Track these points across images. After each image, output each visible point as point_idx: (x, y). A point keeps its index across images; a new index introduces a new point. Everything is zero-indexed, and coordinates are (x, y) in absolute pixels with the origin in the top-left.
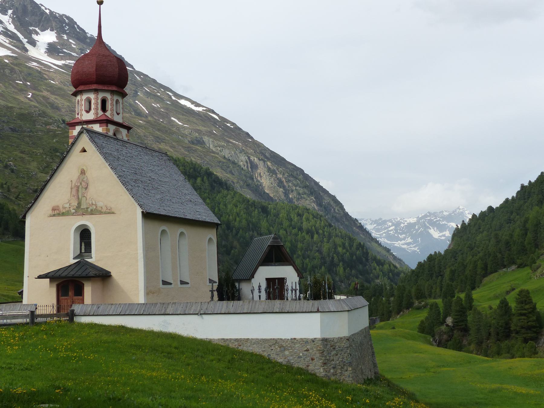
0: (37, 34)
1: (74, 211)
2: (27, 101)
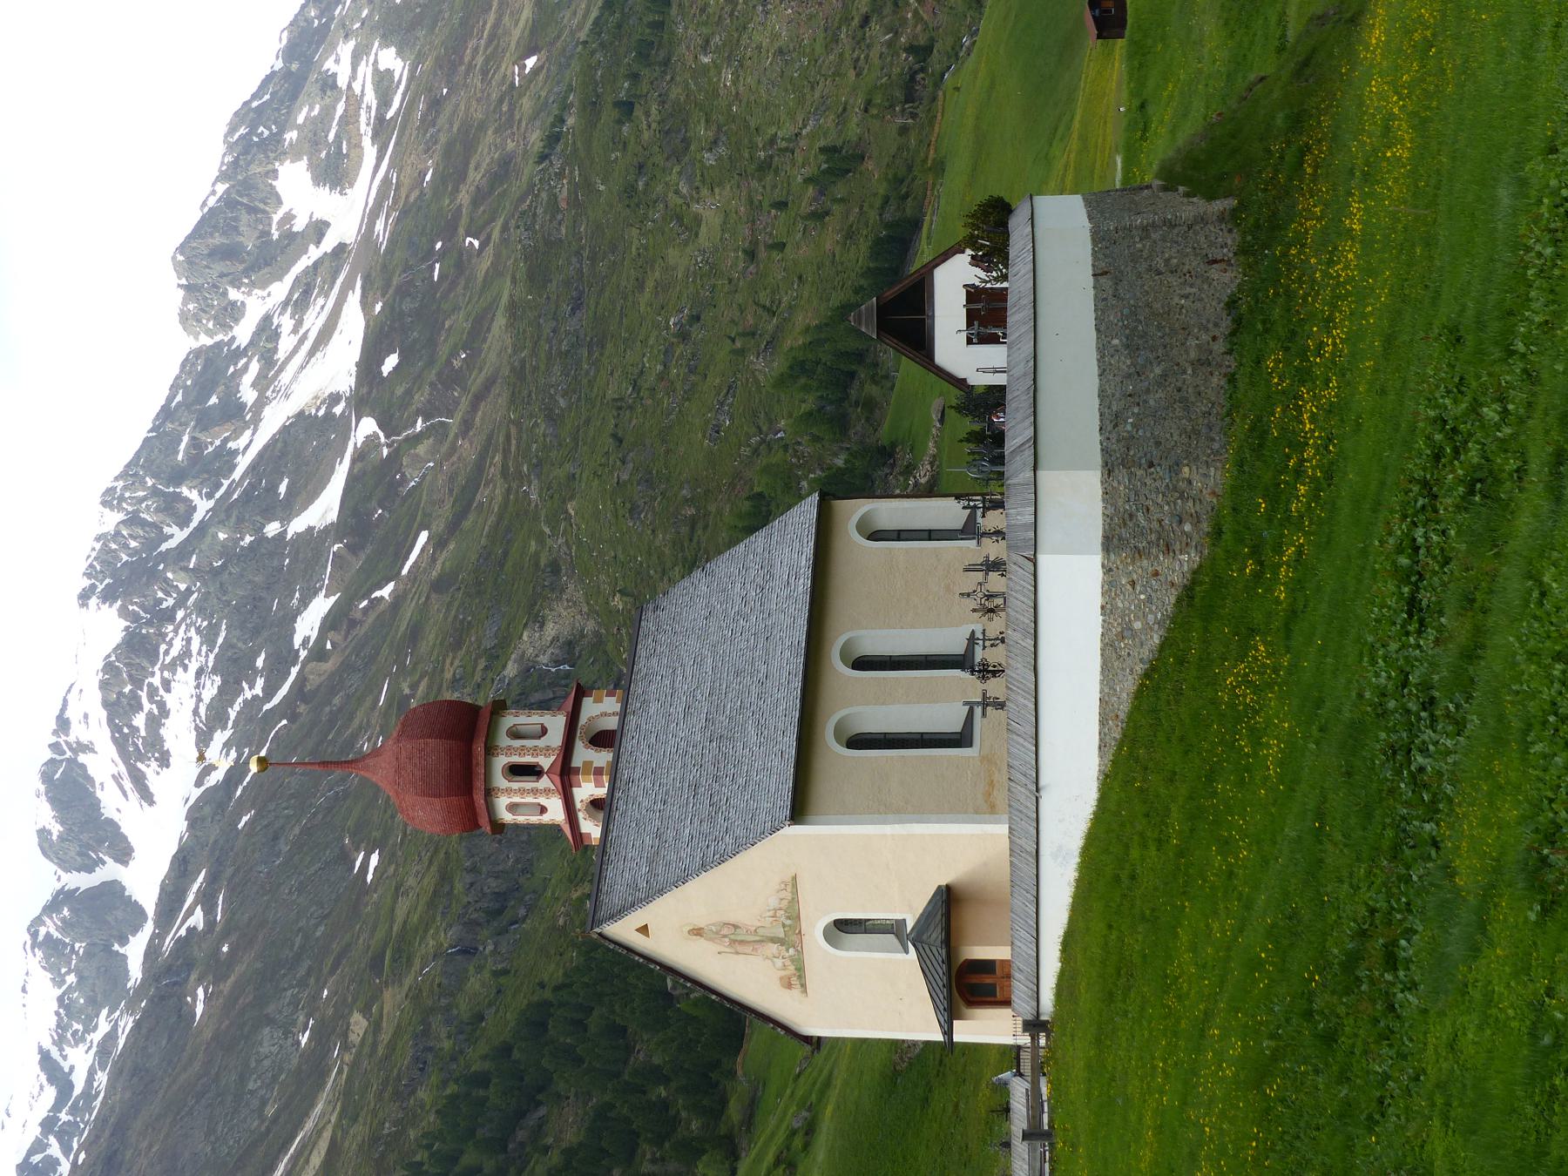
0: (289, 217)
2: (490, 249)
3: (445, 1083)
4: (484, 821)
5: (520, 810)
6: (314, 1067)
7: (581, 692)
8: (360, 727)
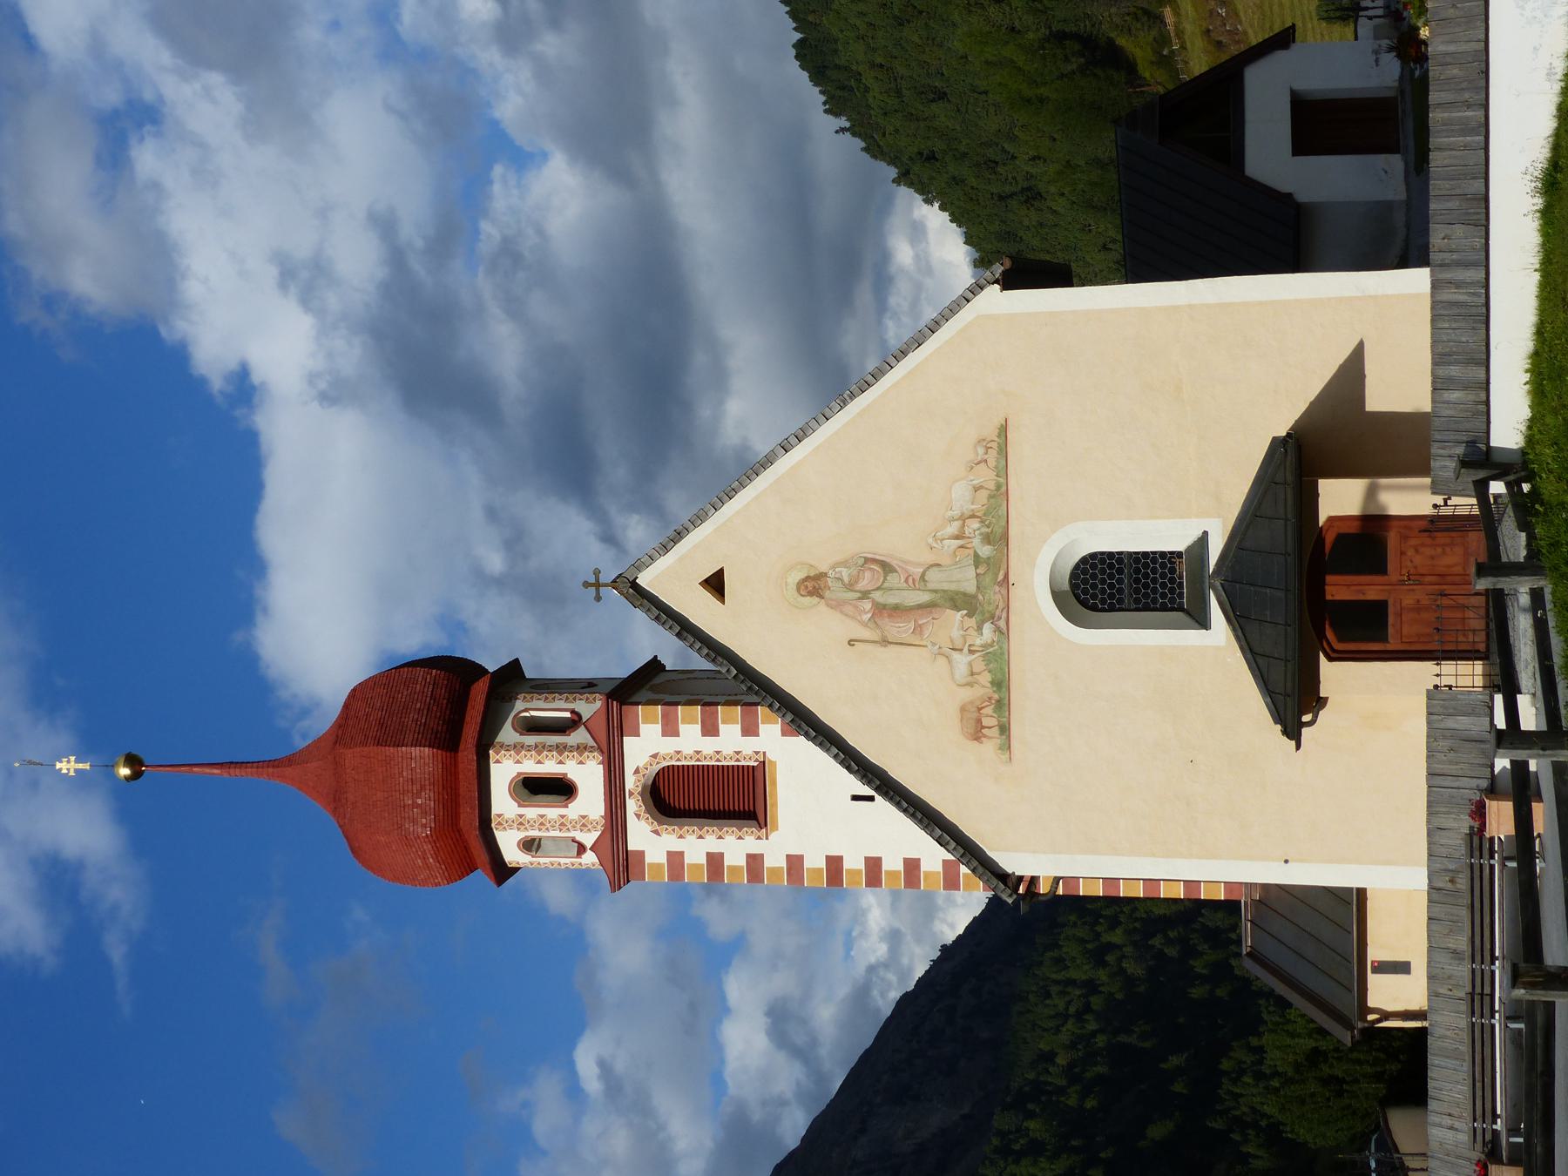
1: (988, 628)
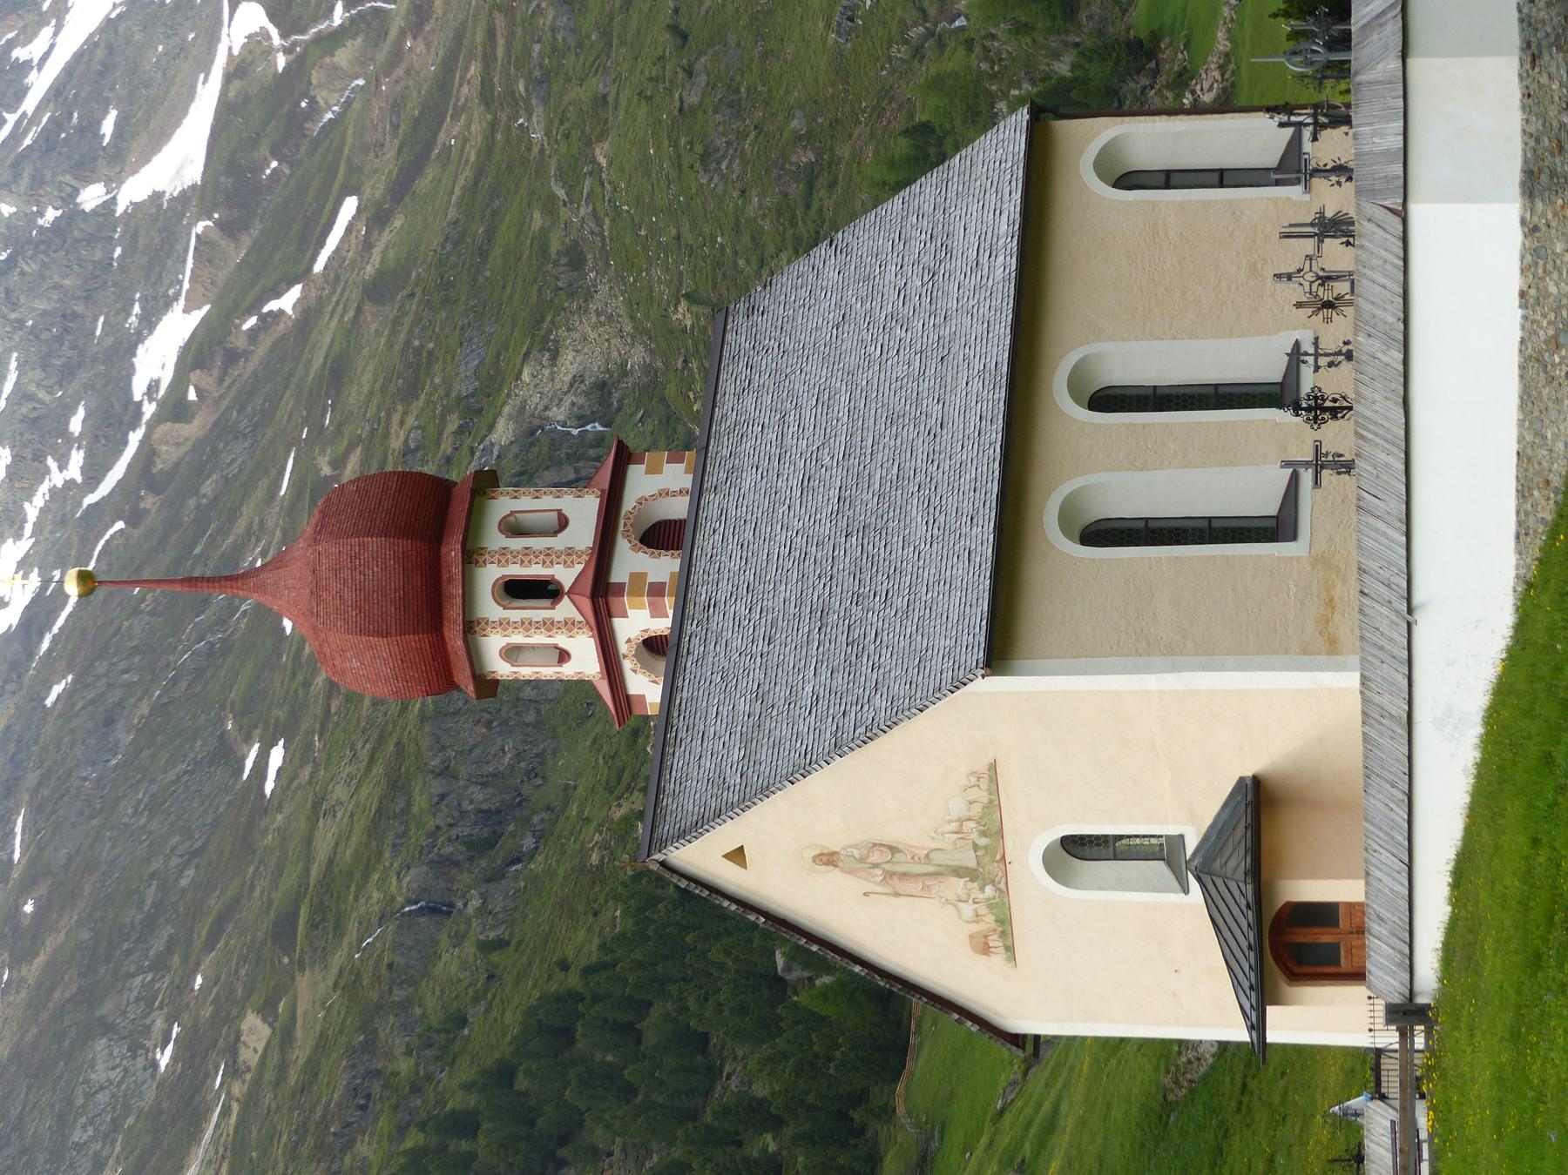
3: (402, 1130)
4: (463, 676)
5: (526, 656)
6: (183, 1104)
7: (624, 458)
8: (249, 532)
